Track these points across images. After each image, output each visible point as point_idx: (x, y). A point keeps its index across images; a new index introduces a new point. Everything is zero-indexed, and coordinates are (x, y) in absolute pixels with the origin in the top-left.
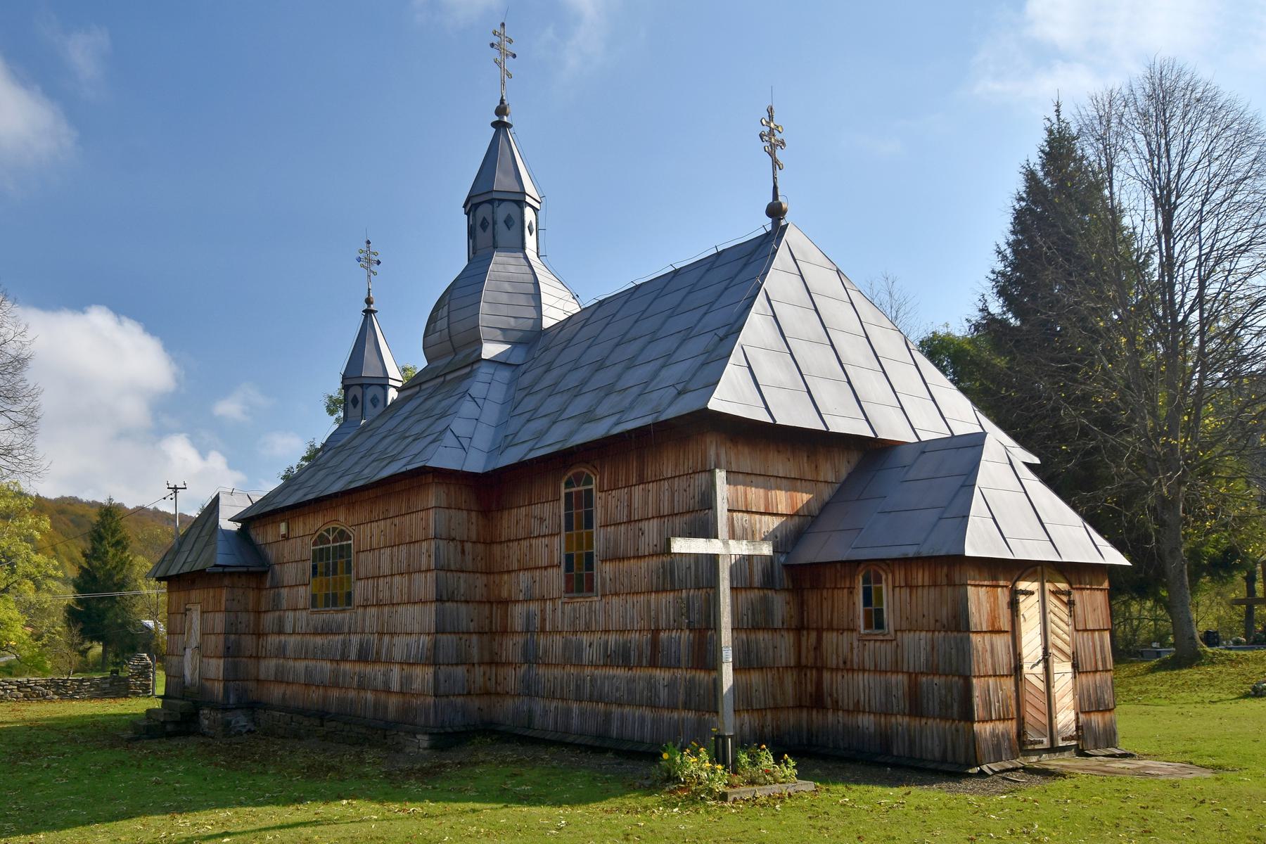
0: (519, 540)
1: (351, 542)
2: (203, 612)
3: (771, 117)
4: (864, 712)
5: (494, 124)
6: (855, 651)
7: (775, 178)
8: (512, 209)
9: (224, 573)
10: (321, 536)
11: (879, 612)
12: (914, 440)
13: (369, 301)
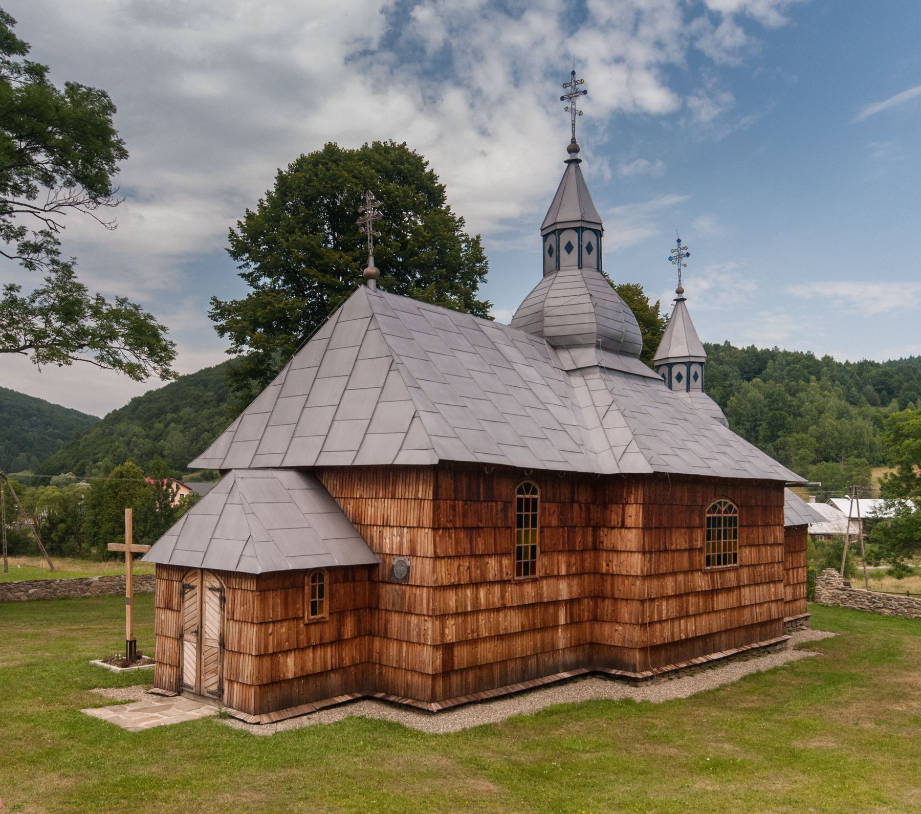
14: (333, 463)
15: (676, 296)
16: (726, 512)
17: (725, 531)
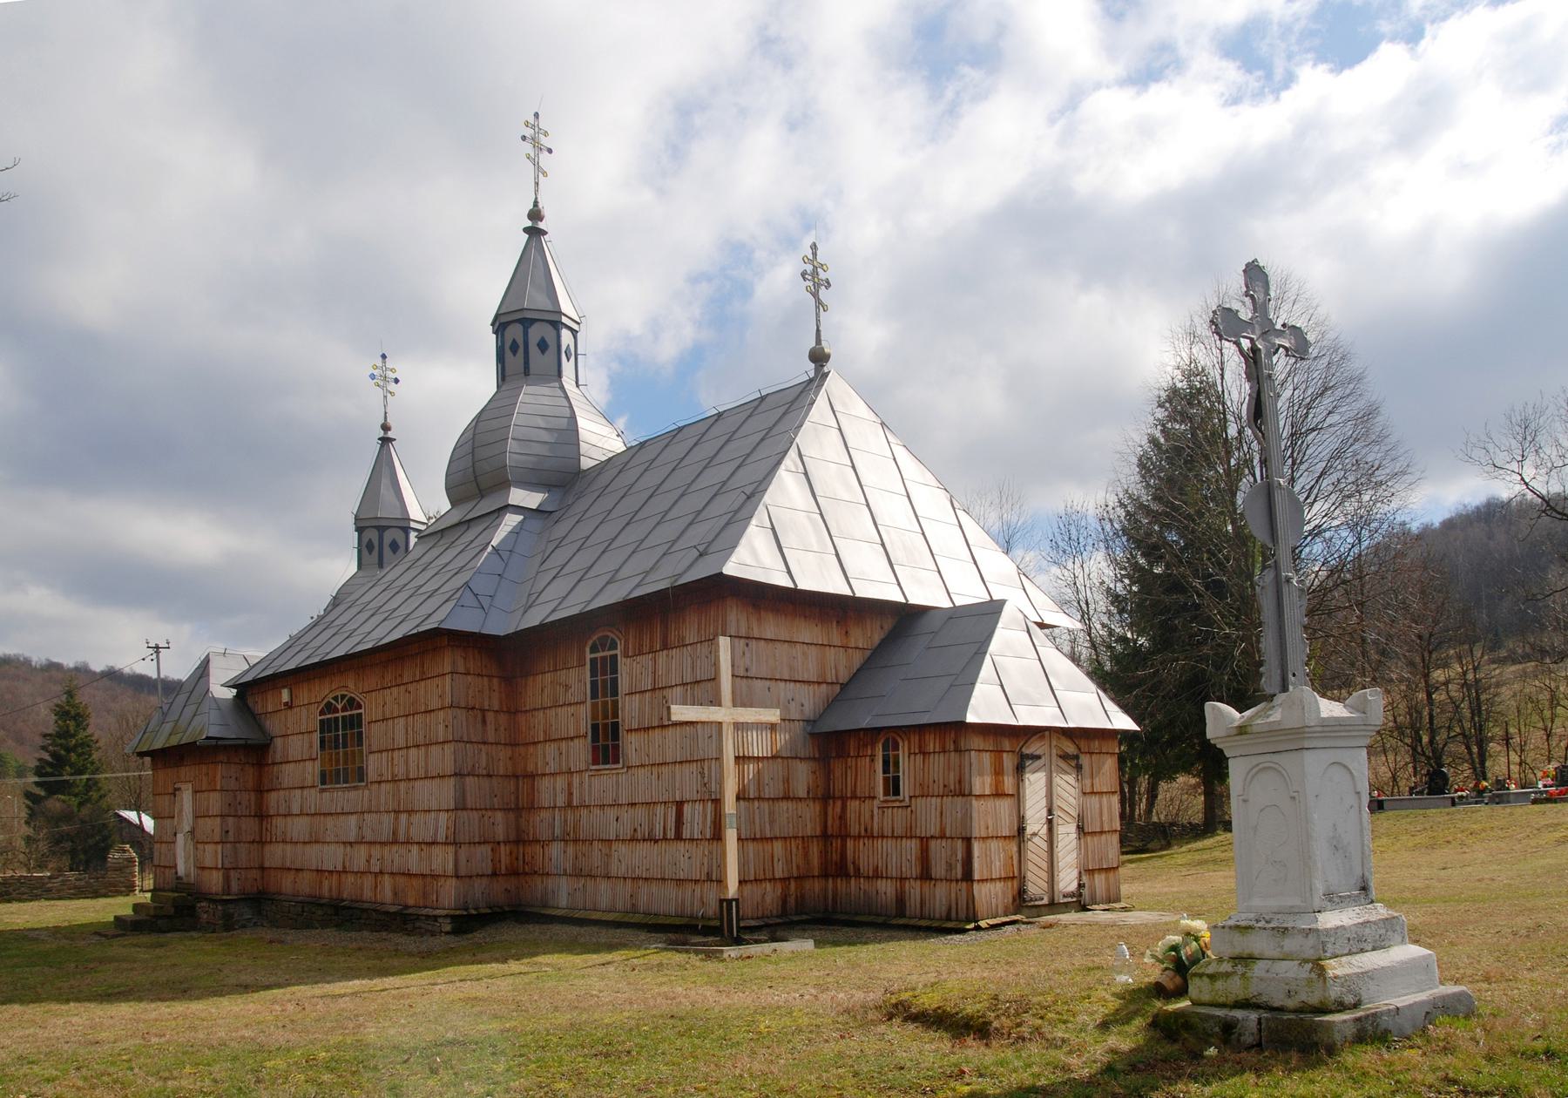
0: (545, 708)
1: (362, 711)
2: (195, 792)
3: (815, 254)
4: (882, 877)
5: (526, 230)
6: (876, 818)
7: (818, 321)
8: (546, 331)
9: (216, 747)
10: (329, 705)
11: (896, 779)
12: (947, 604)
13: (386, 428)
14: (900, 724)
15: (382, 434)
16: (344, 709)
17: (345, 736)
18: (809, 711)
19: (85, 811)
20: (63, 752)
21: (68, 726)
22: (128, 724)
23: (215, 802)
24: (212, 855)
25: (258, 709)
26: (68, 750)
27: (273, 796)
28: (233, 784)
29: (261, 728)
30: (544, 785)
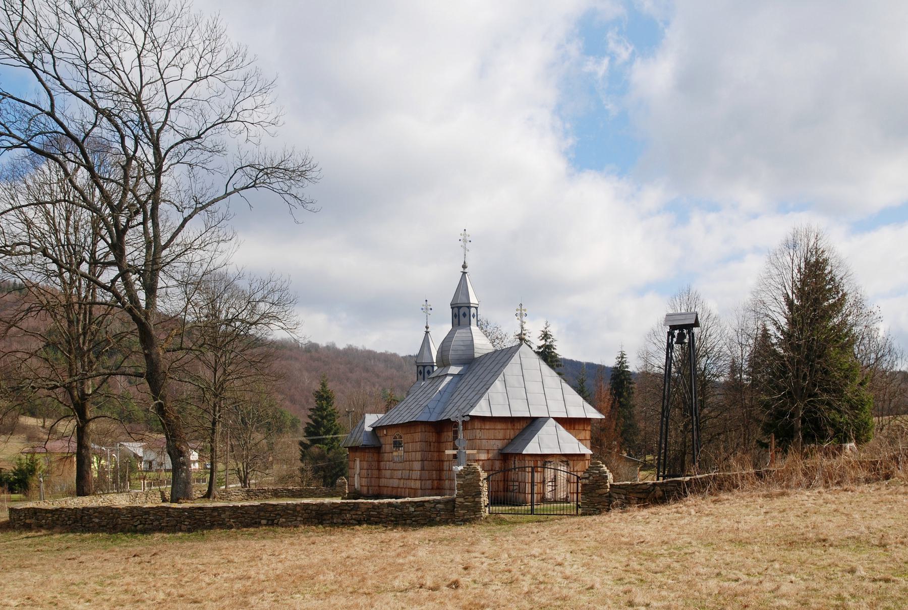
2: (360, 461)
18: (500, 446)
19: (331, 454)
20: (320, 419)
21: (322, 404)
22: (354, 403)
23: (365, 465)
24: (364, 482)
25: (379, 435)
26: (323, 418)
27: (382, 463)
28: (370, 459)
29: (379, 441)
30: (445, 463)
